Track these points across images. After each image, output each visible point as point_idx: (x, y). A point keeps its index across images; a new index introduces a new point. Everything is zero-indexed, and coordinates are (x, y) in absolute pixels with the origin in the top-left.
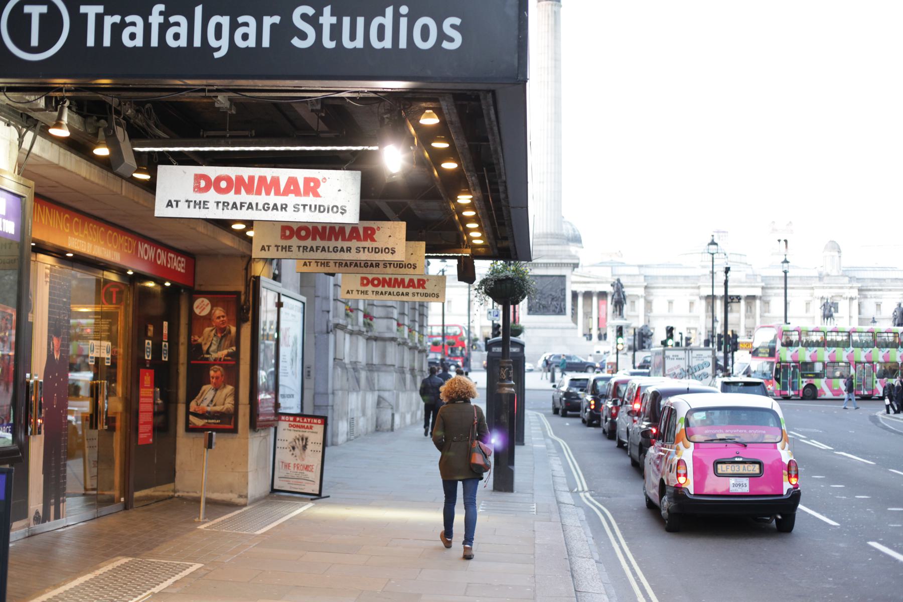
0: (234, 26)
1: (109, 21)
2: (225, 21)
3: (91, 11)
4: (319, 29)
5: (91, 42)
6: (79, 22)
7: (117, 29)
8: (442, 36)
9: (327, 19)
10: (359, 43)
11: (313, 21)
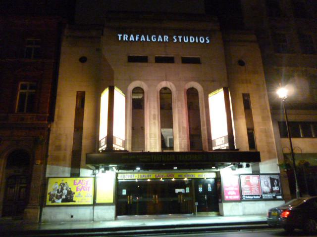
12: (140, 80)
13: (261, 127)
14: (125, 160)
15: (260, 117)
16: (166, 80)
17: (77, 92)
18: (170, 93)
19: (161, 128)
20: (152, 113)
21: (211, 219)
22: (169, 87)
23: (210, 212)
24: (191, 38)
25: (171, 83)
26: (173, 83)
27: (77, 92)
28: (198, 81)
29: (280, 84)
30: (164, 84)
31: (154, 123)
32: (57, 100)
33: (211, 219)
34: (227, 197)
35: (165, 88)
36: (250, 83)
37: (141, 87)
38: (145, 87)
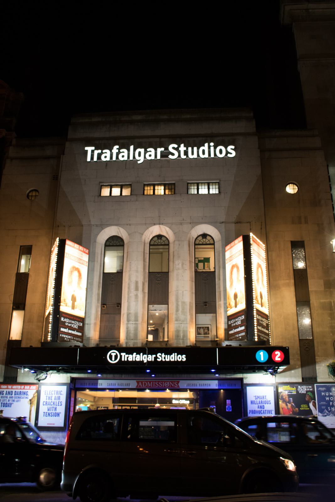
0: (146, 152)
1: (96, 152)
2: (142, 150)
3: (123, 354)
4: (179, 152)
5: (89, 159)
6: (121, 356)
7: (99, 156)
8: (227, 153)
9: (182, 148)
10: (195, 156)
11: (177, 149)
12: (117, 225)
13: (322, 301)
14: (83, 360)
15: (322, 282)
16: (159, 224)
17: (21, 246)
18: (167, 244)
19: (149, 304)
20: (134, 279)
21: (75, 375)
22: (164, 234)
23: (97, 238)
24: (206, 156)
25: (168, 229)
26: (170, 228)
27: (21, 246)
28: (213, 223)
29: (305, 326)
30: (156, 230)
31: (136, 296)
32: (118, 374)
33: (75, 375)
34: (273, 387)
35: (159, 237)
36: (306, 222)
37: (120, 235)
38: (121, 232)
